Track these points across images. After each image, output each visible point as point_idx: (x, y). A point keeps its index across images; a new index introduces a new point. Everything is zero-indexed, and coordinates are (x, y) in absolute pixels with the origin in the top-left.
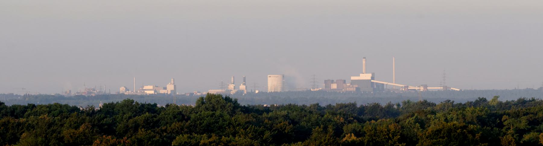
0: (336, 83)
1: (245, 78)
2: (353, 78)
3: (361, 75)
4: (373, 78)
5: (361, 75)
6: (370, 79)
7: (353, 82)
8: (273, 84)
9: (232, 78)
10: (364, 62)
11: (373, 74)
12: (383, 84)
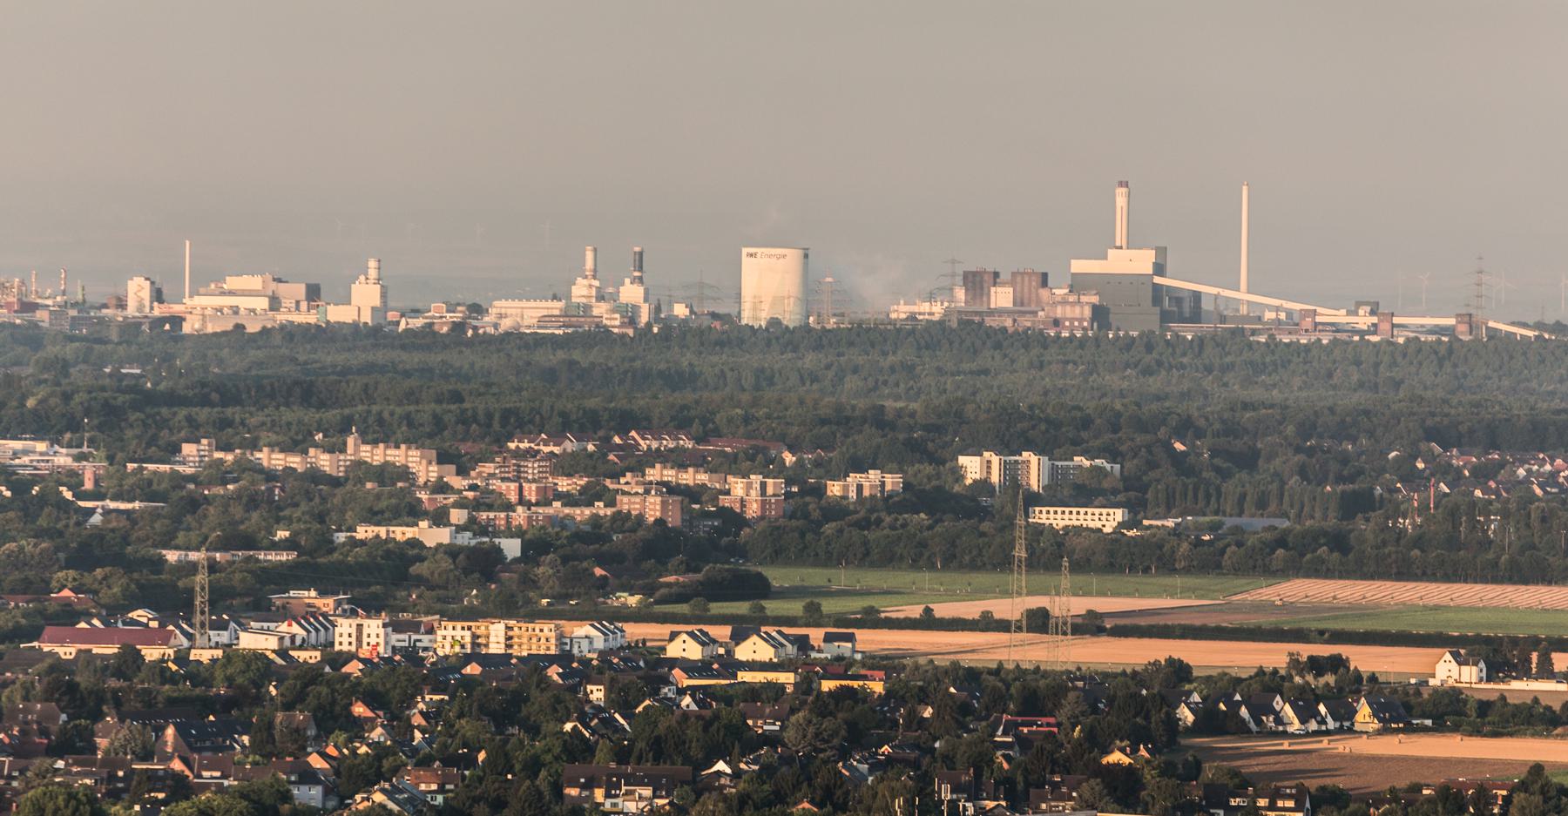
0: (1012, 283)
1: (641, 254)
2: (1079, 266)
4: (1159, 269)
7: (1079, 284)
8: (767, 287)
9: (589, 256)
11: (1161, 252)
12: (1197, 296)
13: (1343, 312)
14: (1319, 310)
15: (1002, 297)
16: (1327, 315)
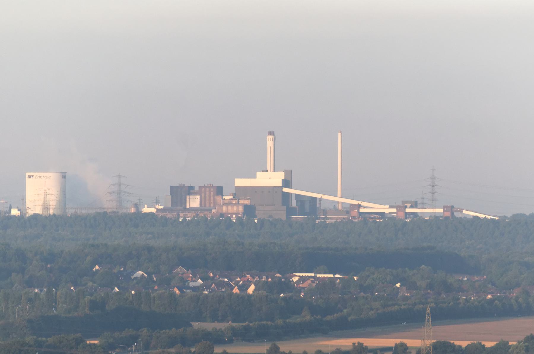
2: (240, 182)
3: (259, 174)
4: (287, 183)
5: (259, 174)
6: (280, 184)
7: (240, 192)
10: (270, 143)
11: (289, 173)
12: (314, 199)
13: (388, 206)
14: (363, 204)
15: (194, 202)
16: (371, 207)
